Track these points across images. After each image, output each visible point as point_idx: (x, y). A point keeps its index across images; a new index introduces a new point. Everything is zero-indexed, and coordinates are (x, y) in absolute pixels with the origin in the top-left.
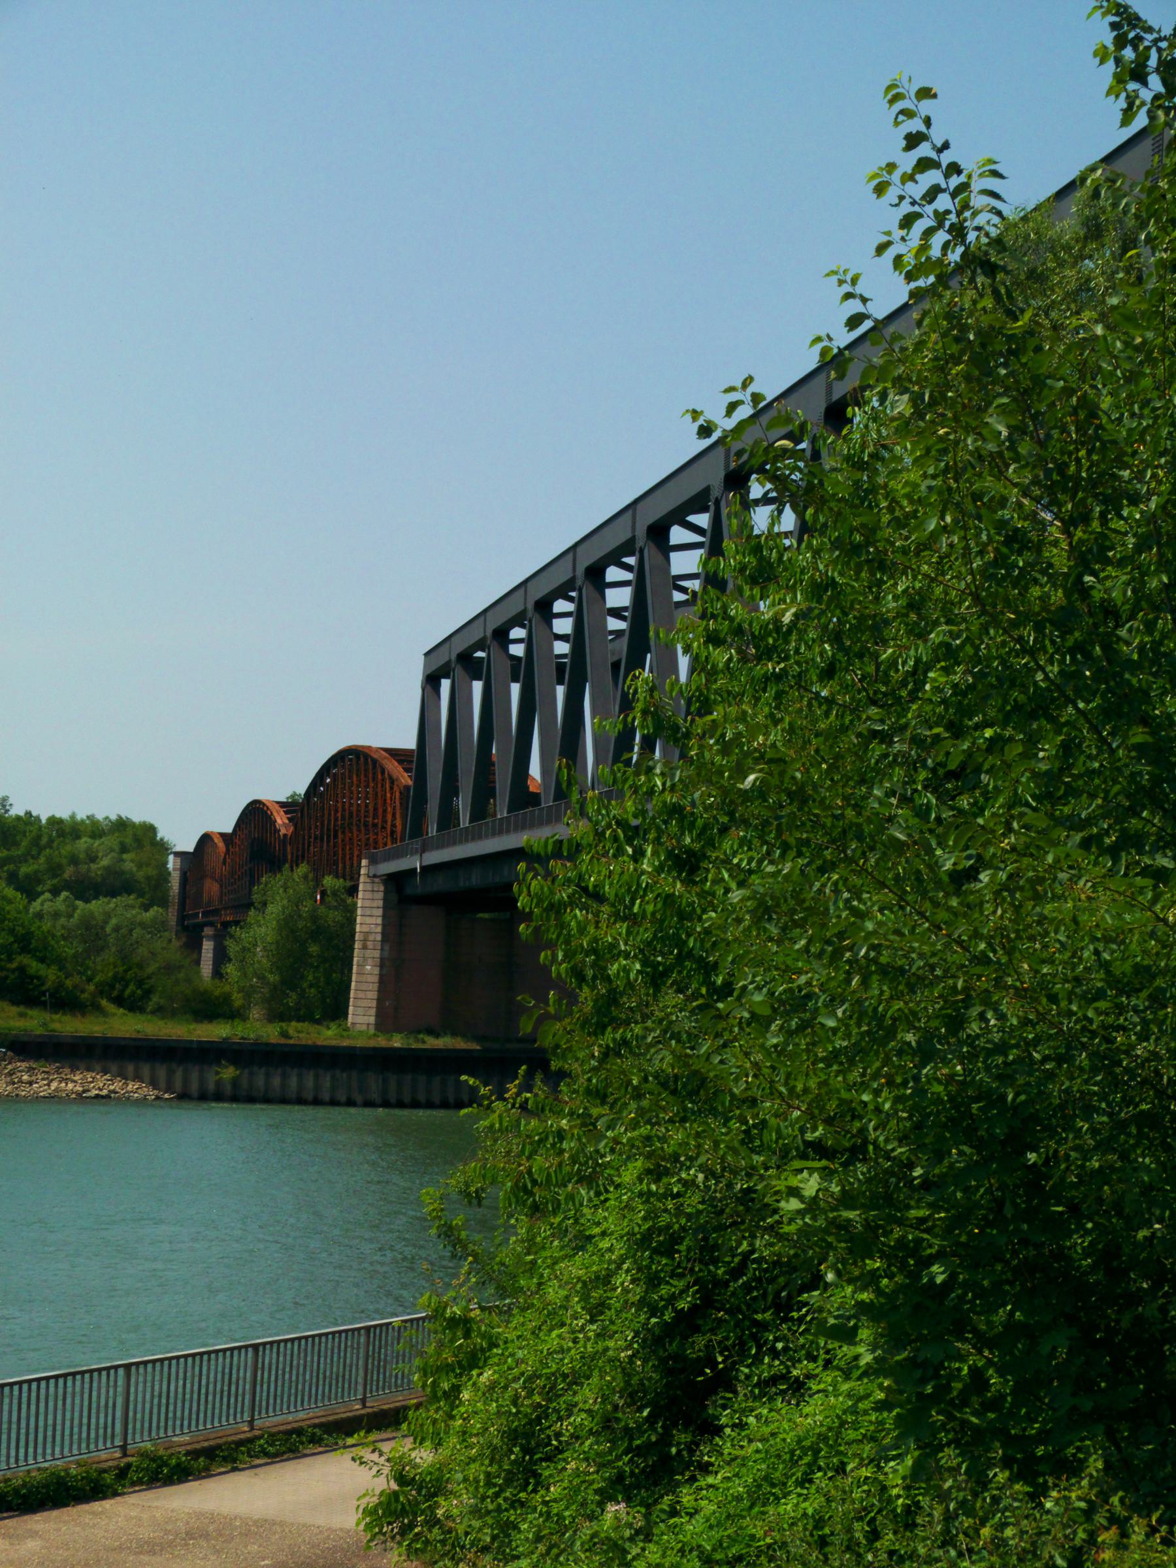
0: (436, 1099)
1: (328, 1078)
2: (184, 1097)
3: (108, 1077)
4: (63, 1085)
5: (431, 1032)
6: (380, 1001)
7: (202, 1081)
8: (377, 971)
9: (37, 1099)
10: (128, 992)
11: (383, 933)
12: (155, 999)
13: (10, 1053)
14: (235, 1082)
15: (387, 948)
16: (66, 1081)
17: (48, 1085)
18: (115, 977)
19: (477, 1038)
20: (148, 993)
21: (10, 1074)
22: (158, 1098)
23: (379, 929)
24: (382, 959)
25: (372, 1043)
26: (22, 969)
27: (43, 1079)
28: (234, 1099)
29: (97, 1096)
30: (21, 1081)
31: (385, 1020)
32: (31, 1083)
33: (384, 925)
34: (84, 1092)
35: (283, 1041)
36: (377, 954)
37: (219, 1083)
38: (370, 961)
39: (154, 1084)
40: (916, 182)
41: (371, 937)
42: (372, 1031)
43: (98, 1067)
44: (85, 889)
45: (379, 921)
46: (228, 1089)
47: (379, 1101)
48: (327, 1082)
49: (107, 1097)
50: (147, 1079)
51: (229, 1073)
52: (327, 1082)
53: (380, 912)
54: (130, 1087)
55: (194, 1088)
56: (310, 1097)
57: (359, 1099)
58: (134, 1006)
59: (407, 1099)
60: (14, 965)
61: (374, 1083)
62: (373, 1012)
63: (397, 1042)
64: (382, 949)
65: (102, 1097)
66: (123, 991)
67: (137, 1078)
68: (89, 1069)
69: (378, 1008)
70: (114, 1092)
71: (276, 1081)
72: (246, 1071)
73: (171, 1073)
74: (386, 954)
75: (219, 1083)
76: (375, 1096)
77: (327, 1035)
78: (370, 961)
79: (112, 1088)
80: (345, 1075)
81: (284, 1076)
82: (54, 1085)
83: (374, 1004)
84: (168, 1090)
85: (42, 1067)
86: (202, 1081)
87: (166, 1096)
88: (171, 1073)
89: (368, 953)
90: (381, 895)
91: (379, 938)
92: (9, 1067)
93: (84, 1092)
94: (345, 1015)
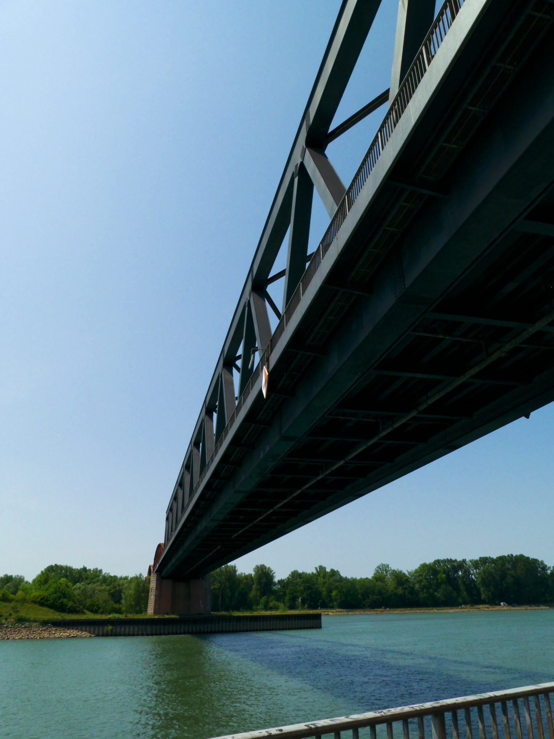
0: (182, 632)
1: (137, 628)
2: (98, 635)
3: (77, 631)
4: (64, 634)
5: (167, 614)
6: (155, 606)
7: (103, 630)
8: (154, 598)
9: (55, 638)
10: (94, 608)
11: (156, 587)
12: (101, 610)
13: (52, 626)
14: (112, 630)
15: (157, 591)
16: (65, 633)
17: (60, 634)
18: (90, 605)
19: (178, 615)
20: (99, 608)
21: (50, 631)
22: (90, 636)
23: (155, 586)
24: (156, 595)
25: (153, 617)
26: (62, 603)
27: (59, 632)
28: (111, 635)
29: (73, 637)
30: (52, 633)
31: (155, 612)
32: (55, 634)
33: (156, 586)
34: (69, 635)
35: (125, 618)
36: (154, 593)
37: (107, 631)
38: (153, 595)
39: (90, 632)
40: (235, 564)
41: (153, 589)
42: (153, 614)
43: (75, 628)
44: (273, 656)
45: (155, 584)
46: (110, 632)
47: (150, 633)
48: (136, 629)
49: (76, 637)
50: (88, 631)
51: (110, 628)
52: (136, 629)
53: (155, 582)
54: (83, 633)
55: (101, 633)
56: (132, 633)
57: (145, 633)
58: (96, 612)
59: (158, 633)
60: (60, 601)
61: (149, 628)
62: (153, 609)
63: (161, 617)
64: (156, 592)
65: (74, 637)
66: (93, 608)
67: (86, 631)
68: (72, 629)
69: (154, 608)
70: (78, 635)
71: (123, 629)
72: (115, 627)
73: (95, 629)
74: (157, 593)
75: (107, 631)
76: (149, 632)
77: (147, 617)
78: (153, 595)
79: (77, 634)
80: (141, 627)
81: (125, 628)
82: (61, 634)
83: (153, 607)
84: (93, 634)
85: (59, 629)
86: (103, 630)
87: (93, 635)
88: (95, 629)
89: (152, 593)
90: (156, 577)
91: (155, 589)
92: (50, 629)
93: (69, 635)
94: (147, 611)
